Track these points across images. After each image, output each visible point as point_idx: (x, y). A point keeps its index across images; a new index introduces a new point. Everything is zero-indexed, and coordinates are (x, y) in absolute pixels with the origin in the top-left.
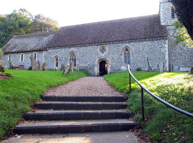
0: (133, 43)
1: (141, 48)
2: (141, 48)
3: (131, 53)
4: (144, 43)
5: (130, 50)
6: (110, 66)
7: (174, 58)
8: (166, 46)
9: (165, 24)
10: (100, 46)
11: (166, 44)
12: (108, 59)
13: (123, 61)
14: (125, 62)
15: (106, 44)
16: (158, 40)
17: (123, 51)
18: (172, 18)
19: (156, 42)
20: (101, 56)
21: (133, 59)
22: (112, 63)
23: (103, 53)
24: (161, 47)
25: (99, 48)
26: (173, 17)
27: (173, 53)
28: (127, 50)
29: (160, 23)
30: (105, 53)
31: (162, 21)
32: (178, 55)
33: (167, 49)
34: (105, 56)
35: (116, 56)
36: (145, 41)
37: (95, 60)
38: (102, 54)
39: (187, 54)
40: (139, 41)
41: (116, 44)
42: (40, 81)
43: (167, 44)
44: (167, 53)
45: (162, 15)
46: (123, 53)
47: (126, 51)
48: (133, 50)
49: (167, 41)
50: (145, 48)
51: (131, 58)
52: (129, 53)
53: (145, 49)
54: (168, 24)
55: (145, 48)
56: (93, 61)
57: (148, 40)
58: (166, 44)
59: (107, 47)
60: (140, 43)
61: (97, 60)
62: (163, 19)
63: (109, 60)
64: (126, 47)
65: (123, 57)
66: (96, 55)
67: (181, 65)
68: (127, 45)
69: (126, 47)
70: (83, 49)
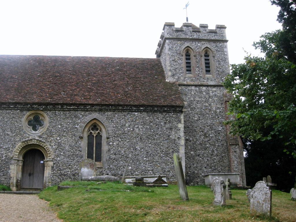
0: (109, 113)
1: (127, 125)
2: (127, 125)
3: (104, 135)
4: (134, 115)
5: (103, 130)
6: (51, 163)
7: (192, 152)
8: (181, 126)
9: (175, 80)
10: (28, 113)
11: (180, 121)
12: (47, 146)
13: (85, 153)
14: (90, 156)
15: (45, 110)
16: (165, 111)
17: (86, 129)
18: (188, 72)
19: (160, 115)
20: (30, 138)
21: (109, 150)
22: (58, 156)
23: (35, 129)
24: (171, 129)
25: (25, 117)
26: (188, 69)
27: (190, 141)
28: (95, 127)
29: (164, 77)
30: (40, 131)
31: (168, 74)
32: (199, 147)
33: (182, 134)
34: (40, 137)
35: (67, 141)
36: (138, 111)
37: (14, 146)
38: (34, 132)
39: (214, 145)
40: (123, 110)
41: (69, 110)
42: (191, 78)
43: (183, 122)
44: (183, 142)
45: (168, 63)
46: (86, 135)
47: (93, 129)
48: (109, 129)
49: (182, 117)
50: (136, 126)
51: (105, 147)
52: (99, 136)
53: (137, 130)
54: (181, 82)
55: (136, 126)
56: (7, 149)
57: (144, 111)
58: (180, 121)
59: (47, 118)
60: (125, 113)
61: (19, 145)
62: (170, 70)
63: (51, 150)
64: (93, 122)
65: (84, 144)
66: (17, 135)
67: (205, 168)
68: (96, 115)
69: (93, 122)
70: (119, 118)
